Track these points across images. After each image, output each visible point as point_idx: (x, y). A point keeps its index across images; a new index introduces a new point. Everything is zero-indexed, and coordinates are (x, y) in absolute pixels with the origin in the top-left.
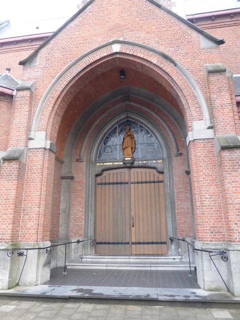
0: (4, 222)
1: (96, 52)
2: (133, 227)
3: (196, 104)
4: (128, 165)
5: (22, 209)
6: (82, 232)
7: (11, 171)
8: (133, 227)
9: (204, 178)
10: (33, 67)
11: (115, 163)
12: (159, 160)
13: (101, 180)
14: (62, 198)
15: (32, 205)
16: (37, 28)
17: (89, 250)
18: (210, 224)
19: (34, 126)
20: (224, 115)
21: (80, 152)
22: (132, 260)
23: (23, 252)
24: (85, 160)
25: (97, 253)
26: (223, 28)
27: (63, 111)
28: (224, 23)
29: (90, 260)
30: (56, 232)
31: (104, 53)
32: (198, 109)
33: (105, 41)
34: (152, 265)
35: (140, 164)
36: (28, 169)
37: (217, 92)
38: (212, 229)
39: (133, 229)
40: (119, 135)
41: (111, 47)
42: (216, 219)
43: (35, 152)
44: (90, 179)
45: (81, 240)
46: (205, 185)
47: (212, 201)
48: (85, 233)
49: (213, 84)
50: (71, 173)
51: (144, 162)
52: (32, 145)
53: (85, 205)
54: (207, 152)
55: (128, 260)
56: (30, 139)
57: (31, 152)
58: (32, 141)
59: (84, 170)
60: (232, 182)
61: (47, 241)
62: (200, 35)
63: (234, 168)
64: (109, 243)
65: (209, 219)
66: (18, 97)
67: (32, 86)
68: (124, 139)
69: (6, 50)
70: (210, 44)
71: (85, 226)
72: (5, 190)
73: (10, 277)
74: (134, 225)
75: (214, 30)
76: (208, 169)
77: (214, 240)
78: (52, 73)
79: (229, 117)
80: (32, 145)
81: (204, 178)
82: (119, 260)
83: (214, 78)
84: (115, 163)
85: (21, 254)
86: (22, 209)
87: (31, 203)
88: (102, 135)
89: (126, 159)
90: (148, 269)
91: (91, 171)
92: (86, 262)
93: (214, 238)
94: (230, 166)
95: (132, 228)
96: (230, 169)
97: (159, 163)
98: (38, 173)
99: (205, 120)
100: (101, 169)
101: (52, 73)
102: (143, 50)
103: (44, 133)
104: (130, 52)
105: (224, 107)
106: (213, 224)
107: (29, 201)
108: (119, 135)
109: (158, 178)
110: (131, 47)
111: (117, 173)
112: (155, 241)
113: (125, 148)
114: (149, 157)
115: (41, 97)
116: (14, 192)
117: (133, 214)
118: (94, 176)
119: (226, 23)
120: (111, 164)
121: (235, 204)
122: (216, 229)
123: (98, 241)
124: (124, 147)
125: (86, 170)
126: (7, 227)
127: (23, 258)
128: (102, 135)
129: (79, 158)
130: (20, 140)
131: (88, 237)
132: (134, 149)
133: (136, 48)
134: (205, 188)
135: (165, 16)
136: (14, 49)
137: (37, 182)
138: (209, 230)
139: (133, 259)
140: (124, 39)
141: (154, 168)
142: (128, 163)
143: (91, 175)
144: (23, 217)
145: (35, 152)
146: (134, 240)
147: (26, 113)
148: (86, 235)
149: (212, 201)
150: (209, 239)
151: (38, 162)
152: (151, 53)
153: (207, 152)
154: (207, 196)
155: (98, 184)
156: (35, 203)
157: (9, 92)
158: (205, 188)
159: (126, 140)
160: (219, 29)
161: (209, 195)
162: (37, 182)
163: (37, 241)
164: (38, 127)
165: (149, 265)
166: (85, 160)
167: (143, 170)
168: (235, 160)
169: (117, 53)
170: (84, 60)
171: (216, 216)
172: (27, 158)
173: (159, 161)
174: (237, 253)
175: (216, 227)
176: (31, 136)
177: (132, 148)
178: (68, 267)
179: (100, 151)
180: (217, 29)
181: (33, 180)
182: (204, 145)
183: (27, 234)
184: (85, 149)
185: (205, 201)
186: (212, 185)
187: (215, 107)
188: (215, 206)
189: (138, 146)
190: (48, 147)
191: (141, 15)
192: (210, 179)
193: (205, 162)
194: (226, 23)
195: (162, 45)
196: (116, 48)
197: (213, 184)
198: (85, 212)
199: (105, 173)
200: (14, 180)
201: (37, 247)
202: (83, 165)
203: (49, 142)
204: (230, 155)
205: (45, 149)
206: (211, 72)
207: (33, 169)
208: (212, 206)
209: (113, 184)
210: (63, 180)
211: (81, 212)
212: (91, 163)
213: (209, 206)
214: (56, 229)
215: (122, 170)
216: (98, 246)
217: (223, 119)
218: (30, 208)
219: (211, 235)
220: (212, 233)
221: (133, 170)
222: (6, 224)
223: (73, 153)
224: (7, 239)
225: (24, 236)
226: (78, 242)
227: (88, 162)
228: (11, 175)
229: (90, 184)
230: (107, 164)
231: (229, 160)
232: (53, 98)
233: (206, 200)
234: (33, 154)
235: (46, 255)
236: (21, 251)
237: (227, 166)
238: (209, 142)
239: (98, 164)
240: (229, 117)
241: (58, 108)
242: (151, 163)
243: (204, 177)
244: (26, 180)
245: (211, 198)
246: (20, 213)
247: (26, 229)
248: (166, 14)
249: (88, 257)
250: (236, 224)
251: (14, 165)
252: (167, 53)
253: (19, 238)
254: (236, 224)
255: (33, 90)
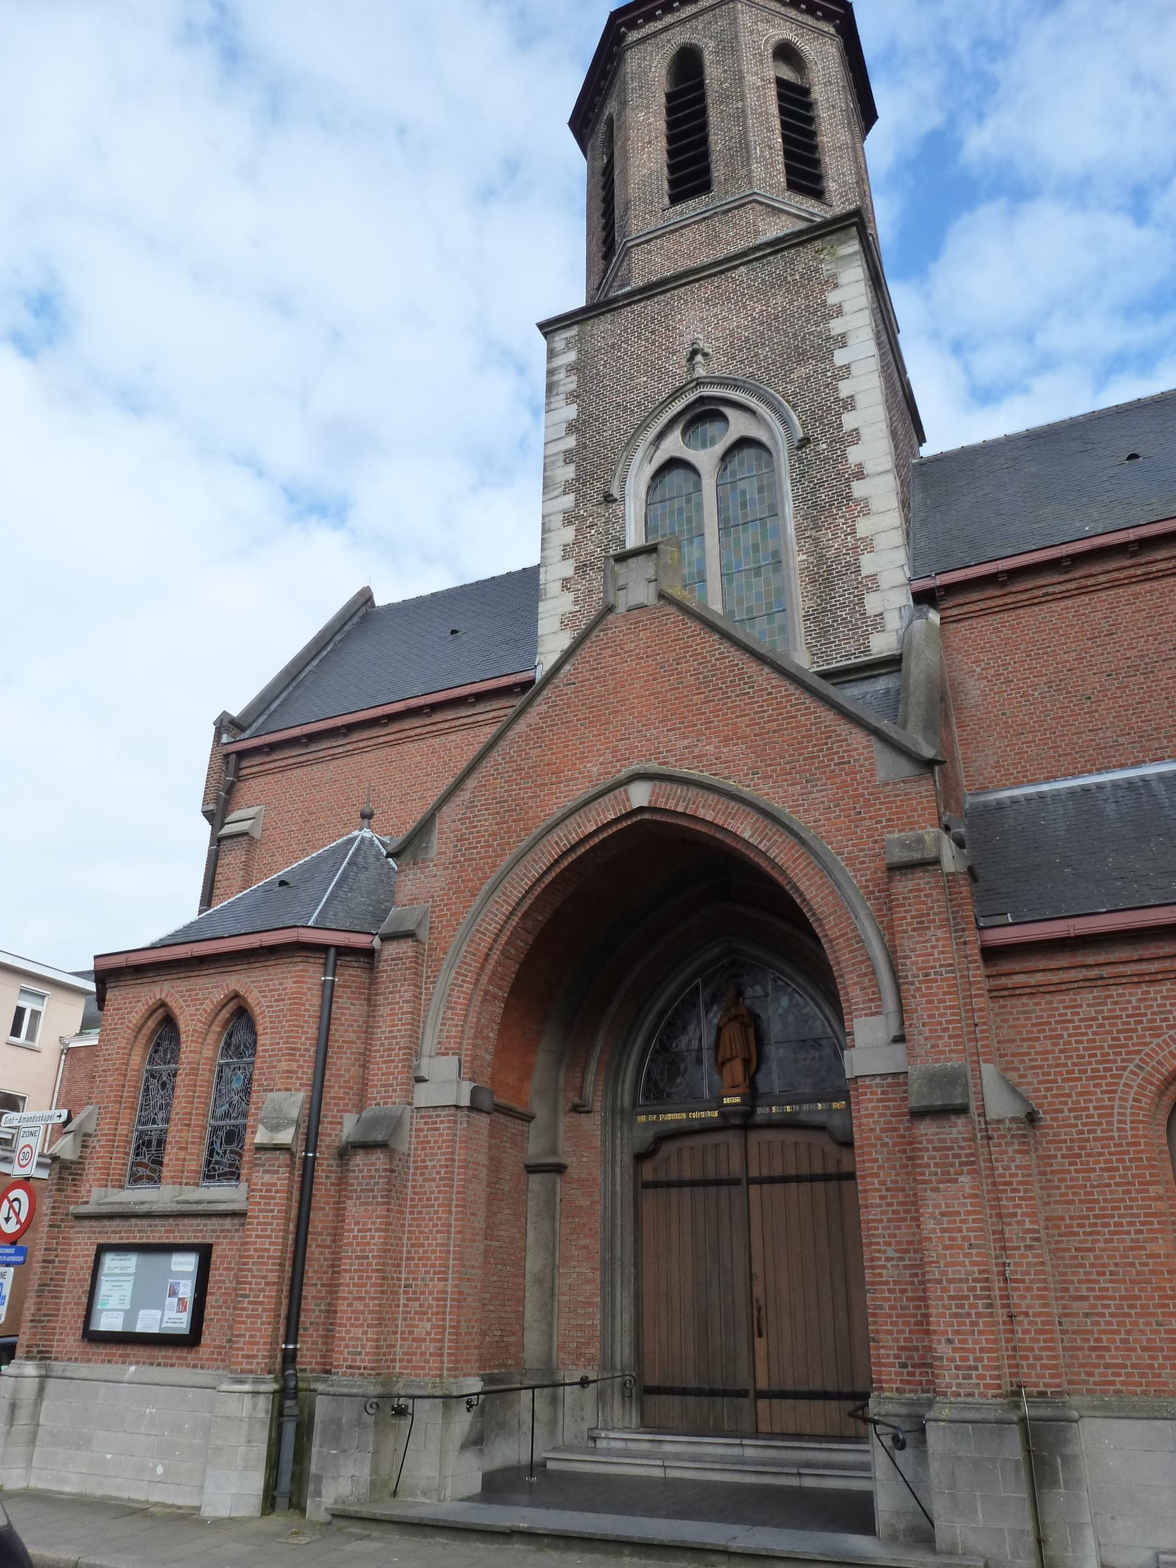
0: (357, 1319)
1: (586, 809)
2: (760, 1335)
3: (862, 962)
4: (735, 1121)
5: (403, 1283)
6: (594, 1350)
7: (371, 1177)
8: (760, 1335)
9: (881, 1198)
10: (424, 861)
11: (695, 1115)
12: (837, 1100)
13: (655, 1169)
14: (531, 1235)
15: (427, 1272)
16: (454, 632)
17: (617, 1404)
18: (897, 1340)
19: (429, 1043)
20: (932, 1002)
21: (583, 1078)
22: (750, 1452)
23: (407, 1406)
24: (598, 1105)
25: (648, 1424)
26: (1045, 607)
27: (506, 985)
28: (1044, 591)
29: (621, 1445)
30: (513, 1350)
31: (607, 812)
32: (866, 979)
33: (609, 773)
34: (802, 1471)
35: (774, 1117)
36: (416, 1168)
37: (914, 930)
38: (904, 1354)
39: (760, 1344)
40: (707, 1012)
41: (626, 792)
42: (916, 1323)
43: (430, 1117)
44: (618, 1170)
45: (591, 1378)
46: (885, 1218)
47: (906, 1267)
48: (604, 1352)
49: (902, 905)
50: (554, 1152)
51: (788, 1109)
52: (424, 1096)
53: (603, 1261)
54: (893, 1115)
55: (736, 1451)
56: (420, 1080)
57: (422, 1117)
58: (424, 1084)
59: (597, 1142)
60: (943, 1214)
61: (470, 1375)
62: (872, 738)
63: (948, 1173)
64: (684, 1392)
65: (894, 1324)
66: (386, 961)
67: (420, 923)
68: (719, 1030)
69: (361, 744)
70: (905, 768)
71: (604, 1328)
72: (359, 1231)
73: (375, 1470)
74: (764, 1332)
75: (1013, 614)
76: (893, 1168)
77: (907, 1387)
78: (472, 880)
79: (946, 1008)
80: (424, 1096)
81: (881, 1198)
82: (709, 1450)
83: (903, 886)
84: (695, 1115)
85: (400, 1412)
86: (403, 1283)
87: (424, 1265)
88: (651, 1017)
89: (726, 1101)
90: (794, 1482)
91: (618, 1142)
92: (609, 1452)
93: (909, 1382)
94: (936, 1165)
95: (757, 1339)
96: (936, 1174)
97: (837, 1110)
98: (440, 1179)
99: (887, 1014)
100: (649, 1135)
101: (472, 880)
102: (712, 798)
103: (453, 1061)
104: (676, 806)
105: (932, 976)
106: (906, 1340)
107: (420, 1259)
108: (707, 1012)
109: (838, 1161)
110: (679, 790)
111: (704, 1146)
112: (835, 1389)
113: (723, 1064)
114: (808, 1090)
115: (445, 953)
116: (377, 1238)
117: (758, 1291)
118: (628, 1159)
119: (1050, 589)
120: (684, 1115)
121: (949, 1281)
122: (915, 1354)
123: (652, 1380)
124: (720, 1059)
125: (604, 1141)
126: (365, 1333)
127: (405, 1422)
128: (651, 1017)
129: (577, 1101)
130: (392, 1085)
131: (613, 1368)
132: (755, 1062)
133: (692, 792)
134: (884, 1228)
135: (774, 682)
136: (381, 740)
137: (439, 1205)
138: (897, 1357)
139: (751, 1451)
140: (660, 764)
141: (821, 1128)
142: (735, 1114)
143: (618, 1158)
144: (405, 1306)
145: (430, 1117)
146: (762, 1384)
147: (406, 1008)
148: (607, 1364)
149: (906, 1267)
150: (894, 1386)
151: (439, 1148)
152: (734, 806)
153: (893, 1115)
154: (891, 1253)
155: (647, 1185)
156: (433, 1266)
157: (361, 941)
158: (884, 1228)
159: (727, 1033)
160: (1028, 610)
161: (897, 1251)
162: (439, 1205)
163: (441, 1376)
164: (439, 1043)
165: (795, 1471)
166: (598, 1105)
167: (790, 1136)
168: (952, 1148)
169: (641, 810)
170: (553, 837)
171: (915, 1316)
172: (410, 1136)
173: (835, 1105)
174: (944, 1427)
175: (916, 1349)
176: (422, 1074)
177: (747, 1062)
178: (551, 1465)
179: (648, 1073)
180: (1021, 611)
181: (429, 1199)
182: (883, 1093)
183: (416, 1354)
184: (596, 1080)
185: (884, 1267)
186: (905, 1220)
187: (907, 977)
188: (912, 1283)
189: (774, 1053)
190: (466, 1101)
191: (706, 683)
192: (901, 1199)
193: (885, 1145)
194: (1050, 589)
195: (765, 778)
196: (640, 795)
197: (909, 1216)
198: (603, 1284)
199: (667, 1149)
200: (378, 1203)
201: (440, 1393)
202: (593, 1124)
203: (467, 1087)
204: (937, 1134)
205: (457, 1107)
206: (897, 869)
207: (426, 1167)
208: (906, 1283)
209: (693, 1183)
210: (534, 1178)
211: (588, 1282)
212: (618, 1116)
213: (895, 1283)
214: (513, 1339)
215: (719, 1138)
216: (653, 1400)
217: (930, 1016)
218: (423, 1279)
219: (901, 1374)
220: (904, 1366)
221: (755, 1137)
222: (362, 1326)
223: (561, 1083)
224: (365, 1368)
225: (409, 1361)
226: (584, 1383)
227: (609, 1115)
228: (372, 1191)
229: (618, 1187)
230: (670, 1117)
231: (935, 1149)
232: (475, 955)
233: (889, 1264)
234: (426, 1123)
235: (469, 1417)
236: (402, 1401)
237: (928, 1165)
238: (898, 1085)
239: (642, 1118)
240: (946, 1008)
241: (490, 982)
242: (809, 1112)
243: (884, 1193)
244: (412, 1200)
245: (902, 1259)
246: (397, 1293)
247: (414, 1340)
248: (776, 679)
249: (612, 1435)
250: (949, 1341)
251: (378, 1160)
252: (778, 805)
253: (398, 1365)
254: (949, 1341)
255: (423, 934)
